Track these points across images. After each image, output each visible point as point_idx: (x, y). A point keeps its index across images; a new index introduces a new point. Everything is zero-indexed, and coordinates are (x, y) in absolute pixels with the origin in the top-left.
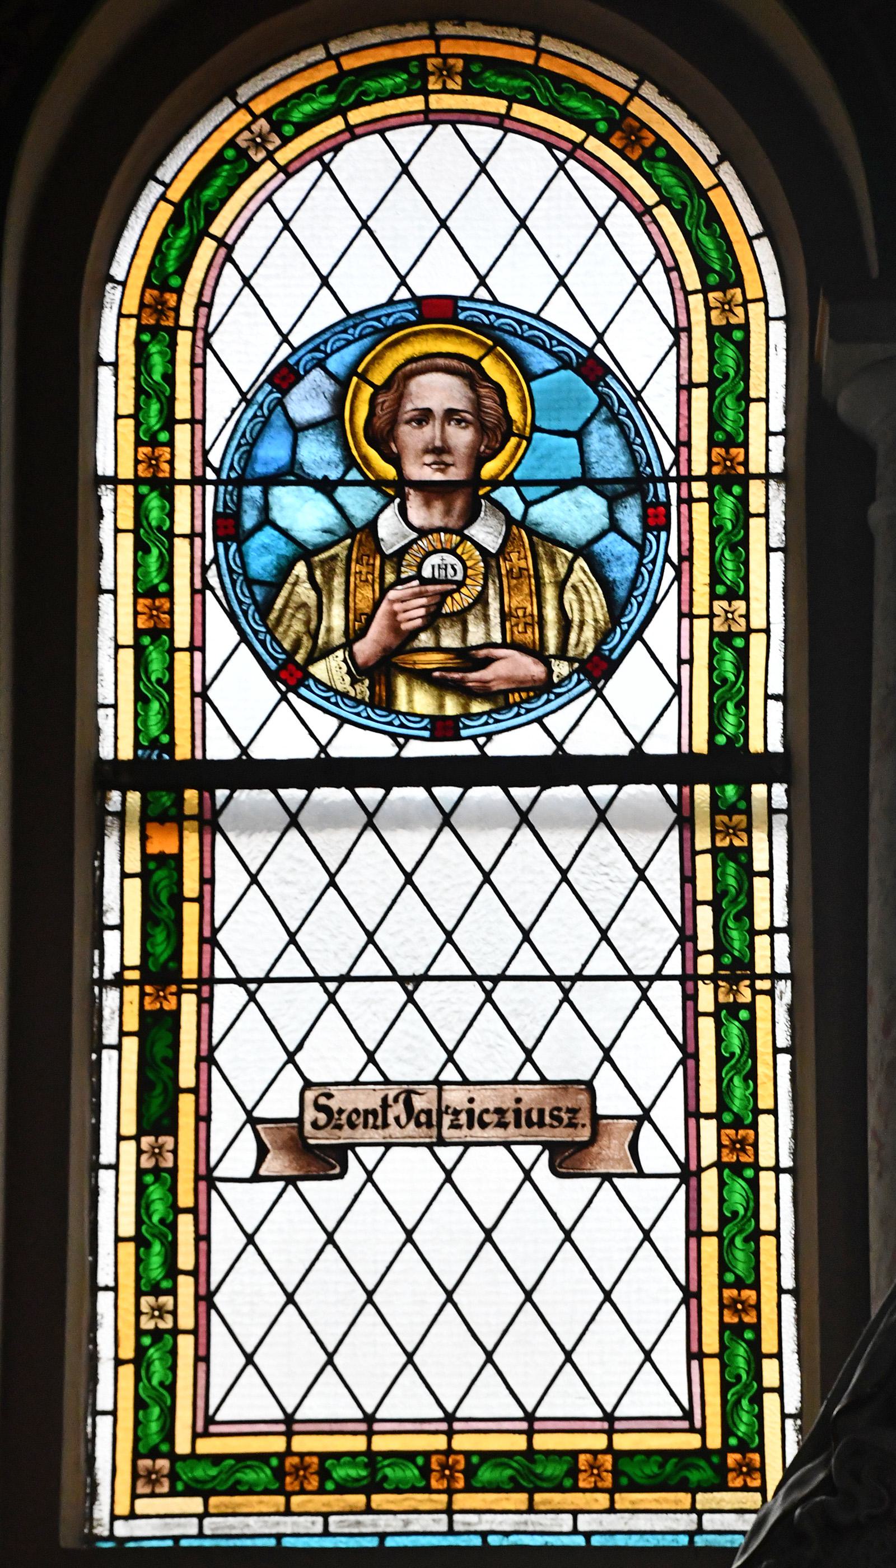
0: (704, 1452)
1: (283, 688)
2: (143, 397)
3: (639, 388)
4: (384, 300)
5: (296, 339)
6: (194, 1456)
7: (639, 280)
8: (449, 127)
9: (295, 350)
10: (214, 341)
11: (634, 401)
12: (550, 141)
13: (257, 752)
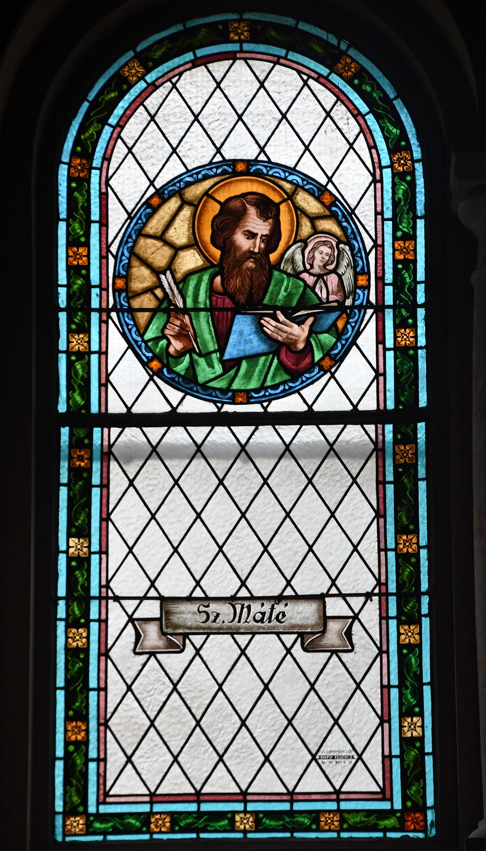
0: (392, 812)
1: (151, 373)
2: (209, 828)
5: (159, 184)
7: (351, 146)
8: (242, 62)
10: (111, 182)
11: (350, 215)
13: (135, 410)
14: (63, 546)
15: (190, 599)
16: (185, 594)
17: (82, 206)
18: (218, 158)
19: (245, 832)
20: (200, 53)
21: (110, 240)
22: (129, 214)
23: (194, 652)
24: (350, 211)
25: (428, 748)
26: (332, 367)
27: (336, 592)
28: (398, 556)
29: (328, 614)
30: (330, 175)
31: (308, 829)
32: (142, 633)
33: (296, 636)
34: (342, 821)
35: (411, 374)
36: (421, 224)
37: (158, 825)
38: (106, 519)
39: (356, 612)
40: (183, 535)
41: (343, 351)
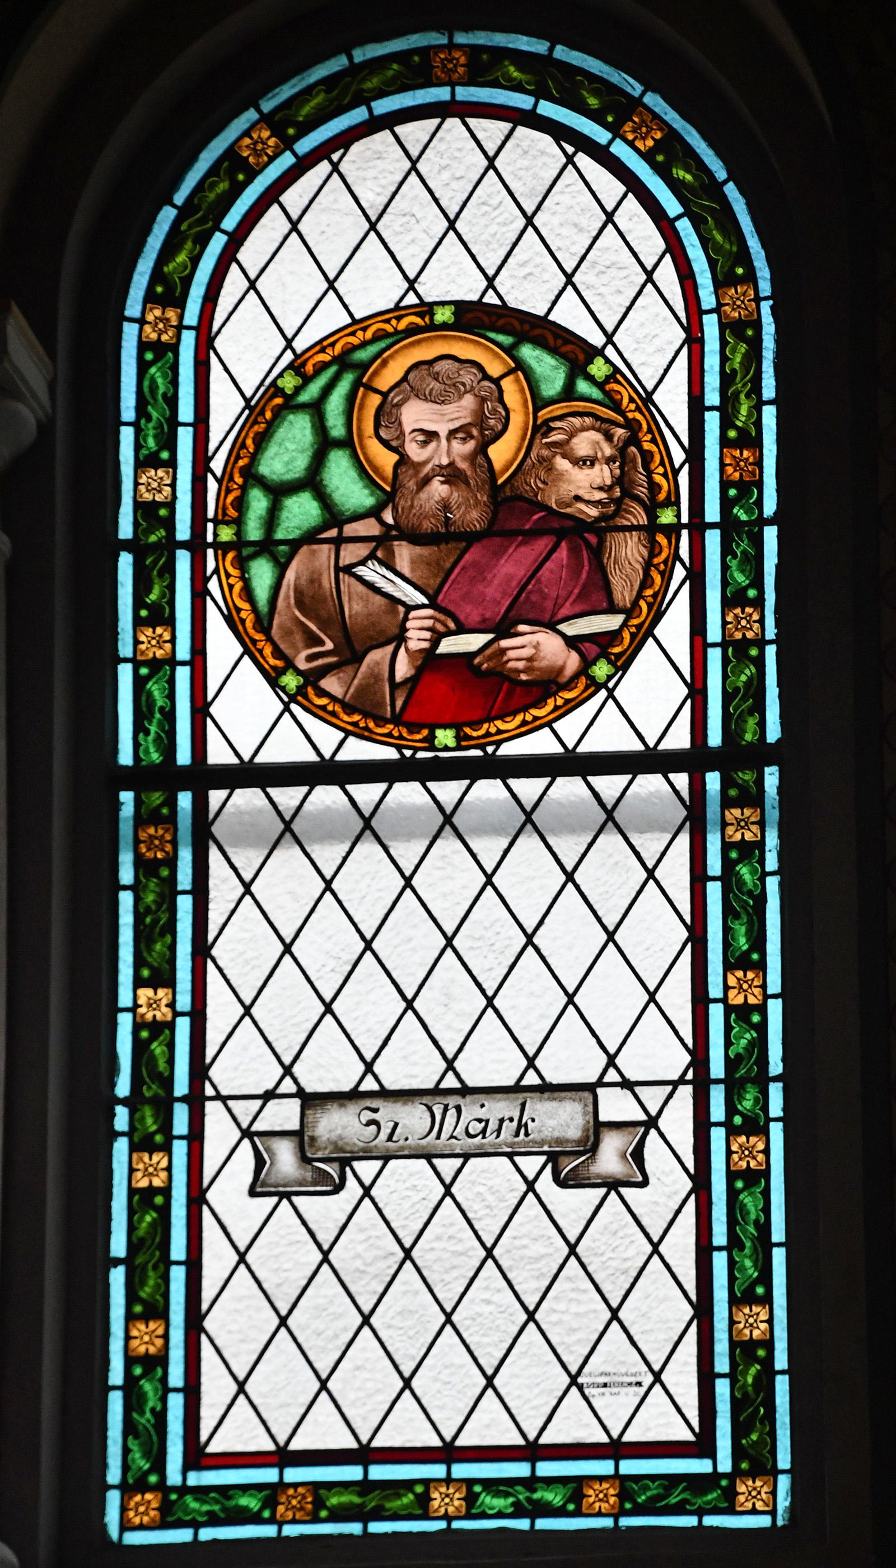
0: (715, 1476)
1: (286, 699)
3: (650, 387)
4: (392, 306)
5: (301, 344)
6: (184, 1490)
7: (649, 275)
9: (297, 356)
12: (559, 132)
14: (125, 998)
15: (354, 1095)
16: (347, 1087)
17: (164, 395)
18: (411, 299)
19: (448, 1518)
20: (383, 106)
21: (212, 446)
22: (247, 401)
23: (360, 1192)
24: (644, 395)
25: (781, 1361)
26: (610, 678)
27: (618, 1079)
28: (729, 1009)
29: (603, 1117)
30: (328, 999)
31: (560, 1512)
32: (266, 1156)
33: (544, 1158)
34: (624, 1495)
35: (735, 711)
36: (769, 415)
37: (299, 1498)
38: (202, 951)
39: (653, 1113)
40: (616, 323)
41: (633, 646)
